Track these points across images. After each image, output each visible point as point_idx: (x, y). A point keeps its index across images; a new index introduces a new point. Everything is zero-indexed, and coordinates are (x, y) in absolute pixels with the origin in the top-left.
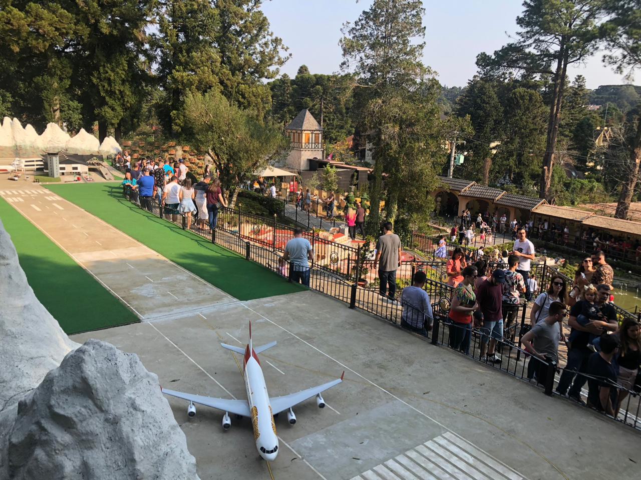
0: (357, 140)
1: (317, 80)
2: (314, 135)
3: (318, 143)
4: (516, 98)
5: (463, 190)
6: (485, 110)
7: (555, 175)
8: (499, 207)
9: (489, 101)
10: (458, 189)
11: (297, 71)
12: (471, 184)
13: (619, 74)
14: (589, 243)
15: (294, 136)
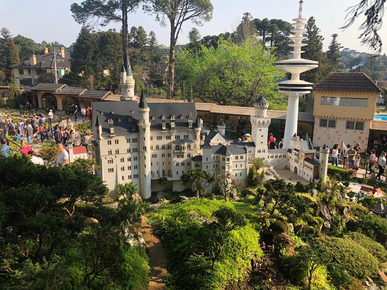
0: (8, 71)
4: (106, 37)
5: (57, 90)
6: (87, 44)
7: (137, 85)
8: (84, 99)
9: (88, 38)
10: (54, 90)
12: (63, 86)
13: (158, 21)
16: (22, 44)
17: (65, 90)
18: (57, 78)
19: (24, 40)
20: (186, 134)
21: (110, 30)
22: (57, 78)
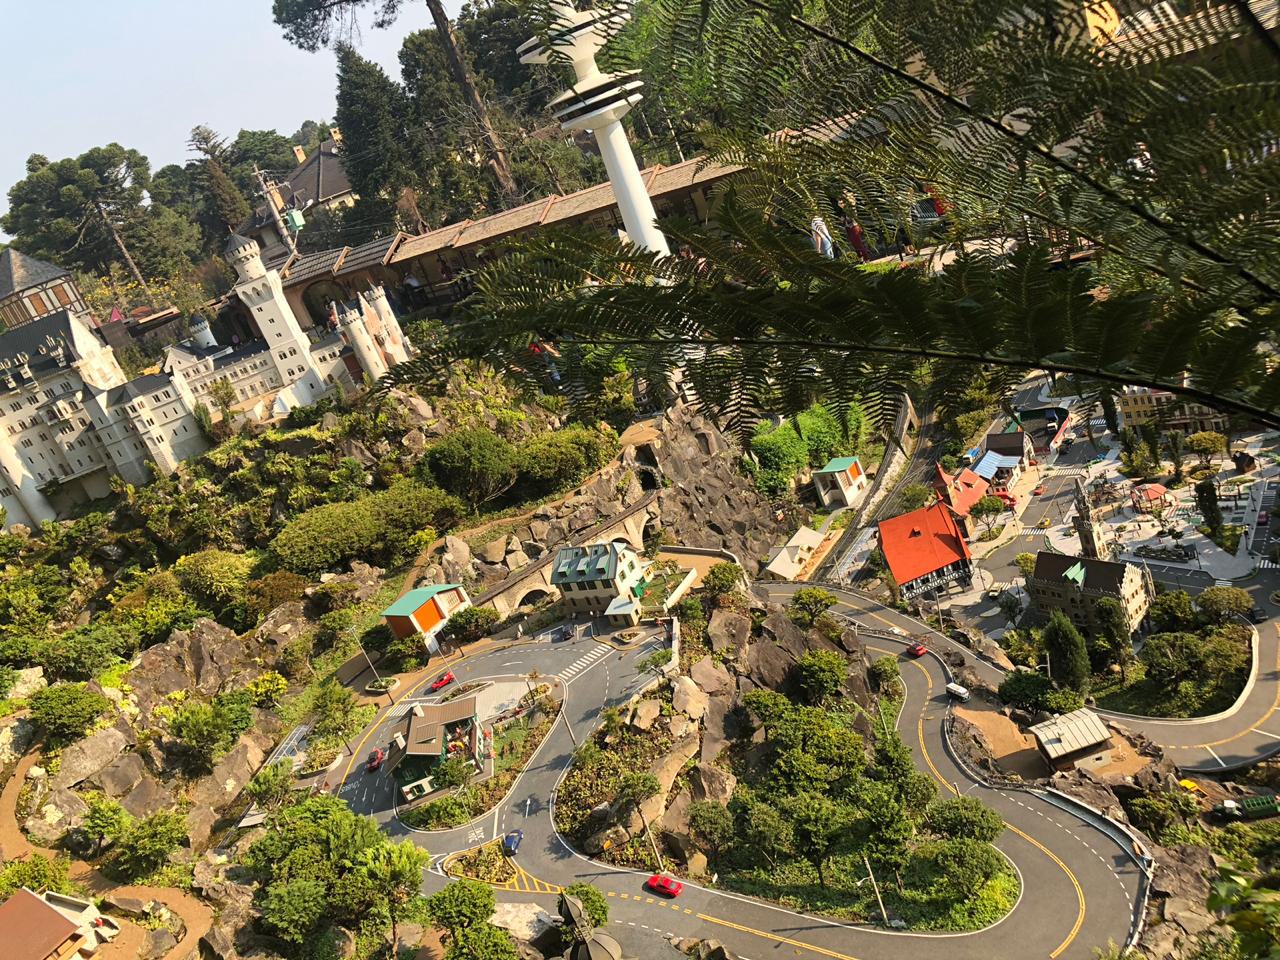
1: (59, 175)
2: (50, 292)
3: (72, 303)
11: (25, 166)
14: (410, 223)
15: (11, 309)
16: (257, 154)
17: (298, 269)
18: (289, 240)
19: (257, 143)
20: (63, 381)
21: (463, 9)
22: (289, 240)
